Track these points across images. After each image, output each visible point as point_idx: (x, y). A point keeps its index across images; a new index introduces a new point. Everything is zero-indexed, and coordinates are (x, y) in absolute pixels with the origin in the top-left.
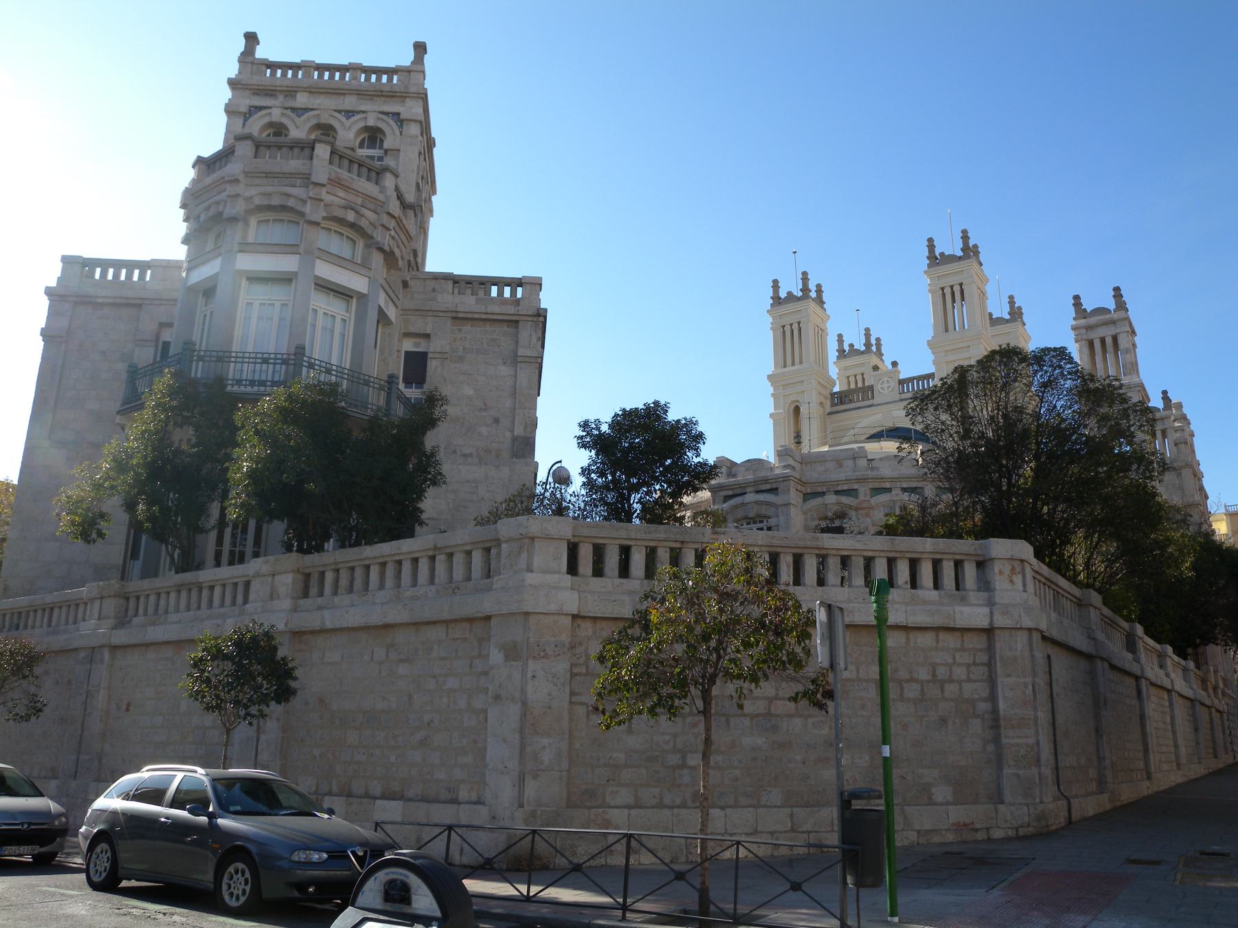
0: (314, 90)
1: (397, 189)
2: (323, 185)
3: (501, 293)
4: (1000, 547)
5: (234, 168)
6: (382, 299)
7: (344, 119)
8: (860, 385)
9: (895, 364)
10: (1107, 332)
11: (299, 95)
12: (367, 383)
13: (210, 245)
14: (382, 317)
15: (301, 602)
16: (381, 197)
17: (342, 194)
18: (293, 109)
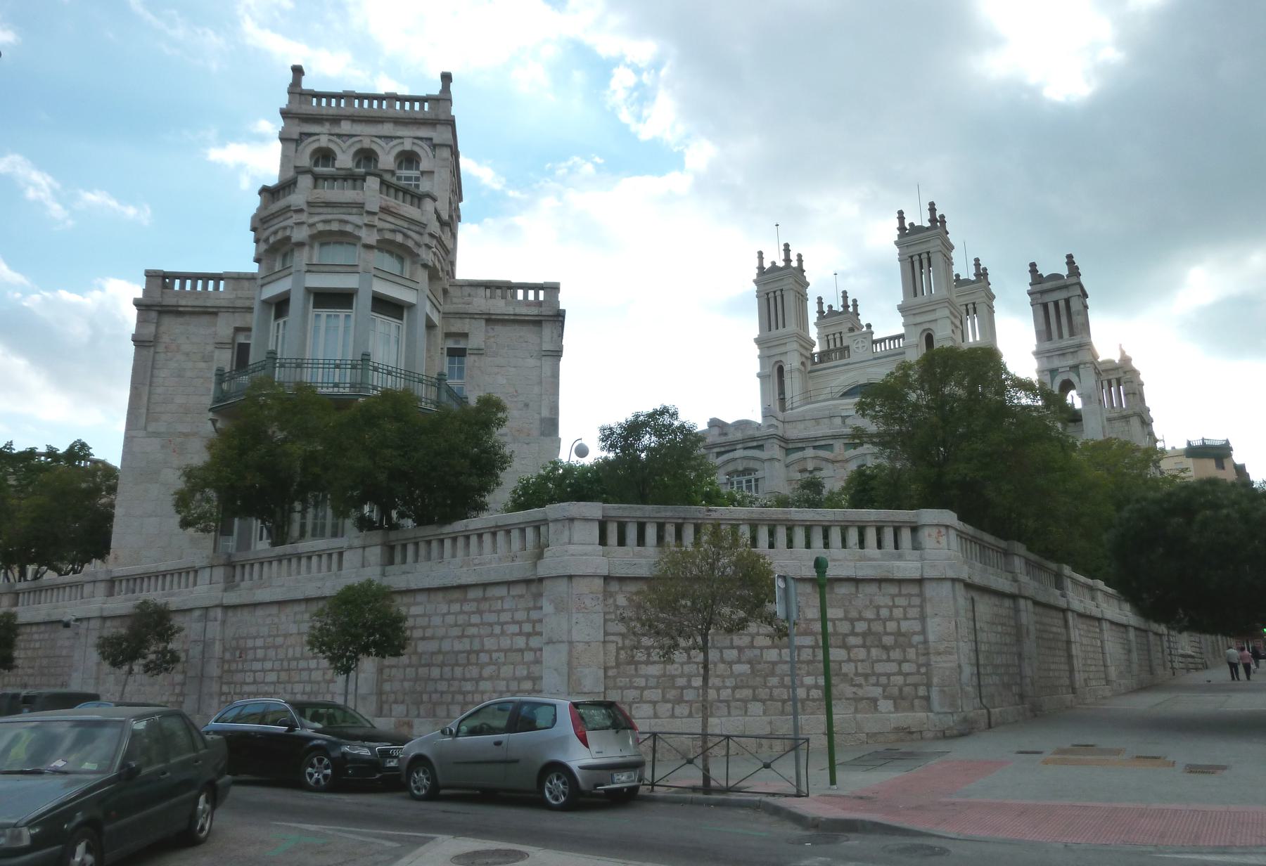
1: (436, 211)
2: (374, 214)
3: (526, 295)
4: (929, 516)
5: (297, 199)
6: (428, 308)
8: (838, 345)
9: (869, 326)
10: (1060, 296)
11: (343, 123)
12: (420, 381)
13: (278, 266)
14: (430, 326)
15: (389, 568)
16: (424, 220)
18: (339, 136)
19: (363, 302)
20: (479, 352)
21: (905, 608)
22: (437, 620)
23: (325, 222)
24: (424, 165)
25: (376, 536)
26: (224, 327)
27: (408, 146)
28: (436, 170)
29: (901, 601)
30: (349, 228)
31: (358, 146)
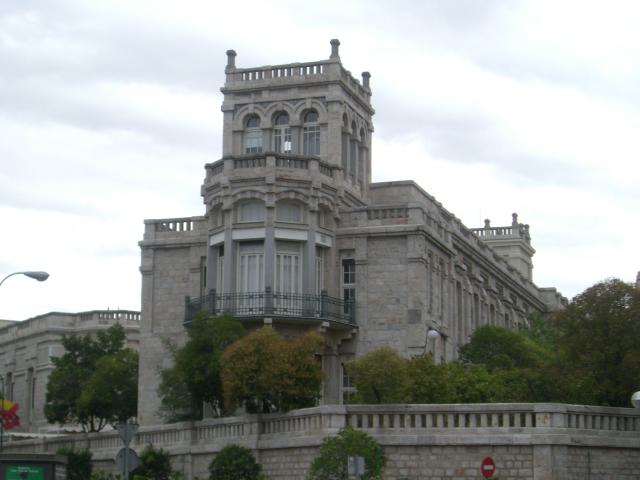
0: (271, 89)
2: (272, 185)
7: (291, 105)
17: (285, 184)
18: (261, 103)
19: (269, 244)
20: (364, 263)
21: (522, 462)
22: (282, 466)
23: (243, 192)
24: (321, 120)
25: (255, 417)
26: (194, 258)
27: (308, 105)
28: (329, 122)
29: (520, 458)
30: (257, 196)
31: (274, 110)
